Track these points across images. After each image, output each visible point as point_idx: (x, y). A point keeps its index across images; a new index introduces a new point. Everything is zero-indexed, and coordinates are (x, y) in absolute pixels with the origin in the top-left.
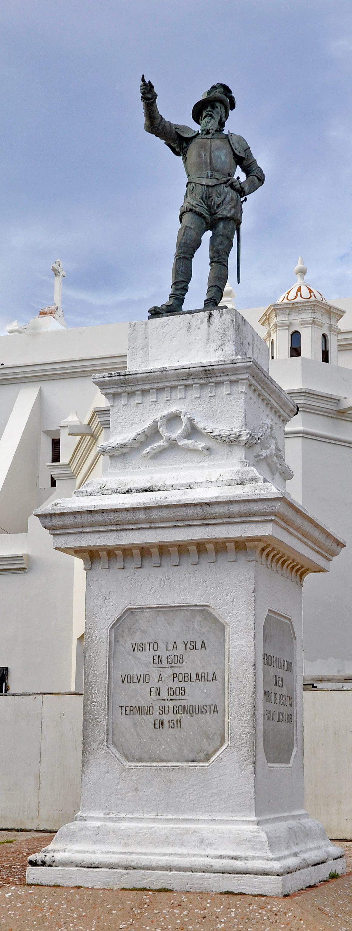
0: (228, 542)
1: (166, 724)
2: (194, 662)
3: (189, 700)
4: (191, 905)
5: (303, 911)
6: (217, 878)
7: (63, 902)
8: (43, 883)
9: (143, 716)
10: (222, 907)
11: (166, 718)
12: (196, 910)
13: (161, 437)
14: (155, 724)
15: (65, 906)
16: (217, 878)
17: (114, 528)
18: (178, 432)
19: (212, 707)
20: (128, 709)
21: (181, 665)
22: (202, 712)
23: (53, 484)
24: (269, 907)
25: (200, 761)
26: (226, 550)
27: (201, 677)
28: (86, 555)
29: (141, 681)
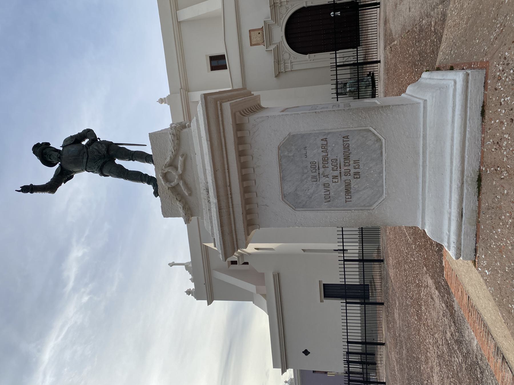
0: (237, 135)
1: (356, 170)
2: (315, 154)
3: (341, 158)
4: (498, 134)
5: (503, 44)
6: (471, 121)
7: (494, 232)
8: (474, 247)
9: (352, 186)
10: (499, 110)
11: (353, 171)
12: (504, 128)
13: (178, 184)
14: (357, 178)
15: (499, 230)
16: (471, 121)
17: (231, 209)
18: (174, 175)
19: (345, 139)
20: (347, 197)
21: (317, 163)
22: (348, 146)
23: (247, 263)
24: (498, 74)
25: (381, 146)
26: (242, 137)
27: (325, 148)
28: (250, 228)
29: (328, 189)
